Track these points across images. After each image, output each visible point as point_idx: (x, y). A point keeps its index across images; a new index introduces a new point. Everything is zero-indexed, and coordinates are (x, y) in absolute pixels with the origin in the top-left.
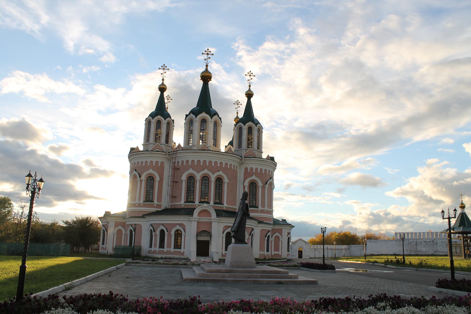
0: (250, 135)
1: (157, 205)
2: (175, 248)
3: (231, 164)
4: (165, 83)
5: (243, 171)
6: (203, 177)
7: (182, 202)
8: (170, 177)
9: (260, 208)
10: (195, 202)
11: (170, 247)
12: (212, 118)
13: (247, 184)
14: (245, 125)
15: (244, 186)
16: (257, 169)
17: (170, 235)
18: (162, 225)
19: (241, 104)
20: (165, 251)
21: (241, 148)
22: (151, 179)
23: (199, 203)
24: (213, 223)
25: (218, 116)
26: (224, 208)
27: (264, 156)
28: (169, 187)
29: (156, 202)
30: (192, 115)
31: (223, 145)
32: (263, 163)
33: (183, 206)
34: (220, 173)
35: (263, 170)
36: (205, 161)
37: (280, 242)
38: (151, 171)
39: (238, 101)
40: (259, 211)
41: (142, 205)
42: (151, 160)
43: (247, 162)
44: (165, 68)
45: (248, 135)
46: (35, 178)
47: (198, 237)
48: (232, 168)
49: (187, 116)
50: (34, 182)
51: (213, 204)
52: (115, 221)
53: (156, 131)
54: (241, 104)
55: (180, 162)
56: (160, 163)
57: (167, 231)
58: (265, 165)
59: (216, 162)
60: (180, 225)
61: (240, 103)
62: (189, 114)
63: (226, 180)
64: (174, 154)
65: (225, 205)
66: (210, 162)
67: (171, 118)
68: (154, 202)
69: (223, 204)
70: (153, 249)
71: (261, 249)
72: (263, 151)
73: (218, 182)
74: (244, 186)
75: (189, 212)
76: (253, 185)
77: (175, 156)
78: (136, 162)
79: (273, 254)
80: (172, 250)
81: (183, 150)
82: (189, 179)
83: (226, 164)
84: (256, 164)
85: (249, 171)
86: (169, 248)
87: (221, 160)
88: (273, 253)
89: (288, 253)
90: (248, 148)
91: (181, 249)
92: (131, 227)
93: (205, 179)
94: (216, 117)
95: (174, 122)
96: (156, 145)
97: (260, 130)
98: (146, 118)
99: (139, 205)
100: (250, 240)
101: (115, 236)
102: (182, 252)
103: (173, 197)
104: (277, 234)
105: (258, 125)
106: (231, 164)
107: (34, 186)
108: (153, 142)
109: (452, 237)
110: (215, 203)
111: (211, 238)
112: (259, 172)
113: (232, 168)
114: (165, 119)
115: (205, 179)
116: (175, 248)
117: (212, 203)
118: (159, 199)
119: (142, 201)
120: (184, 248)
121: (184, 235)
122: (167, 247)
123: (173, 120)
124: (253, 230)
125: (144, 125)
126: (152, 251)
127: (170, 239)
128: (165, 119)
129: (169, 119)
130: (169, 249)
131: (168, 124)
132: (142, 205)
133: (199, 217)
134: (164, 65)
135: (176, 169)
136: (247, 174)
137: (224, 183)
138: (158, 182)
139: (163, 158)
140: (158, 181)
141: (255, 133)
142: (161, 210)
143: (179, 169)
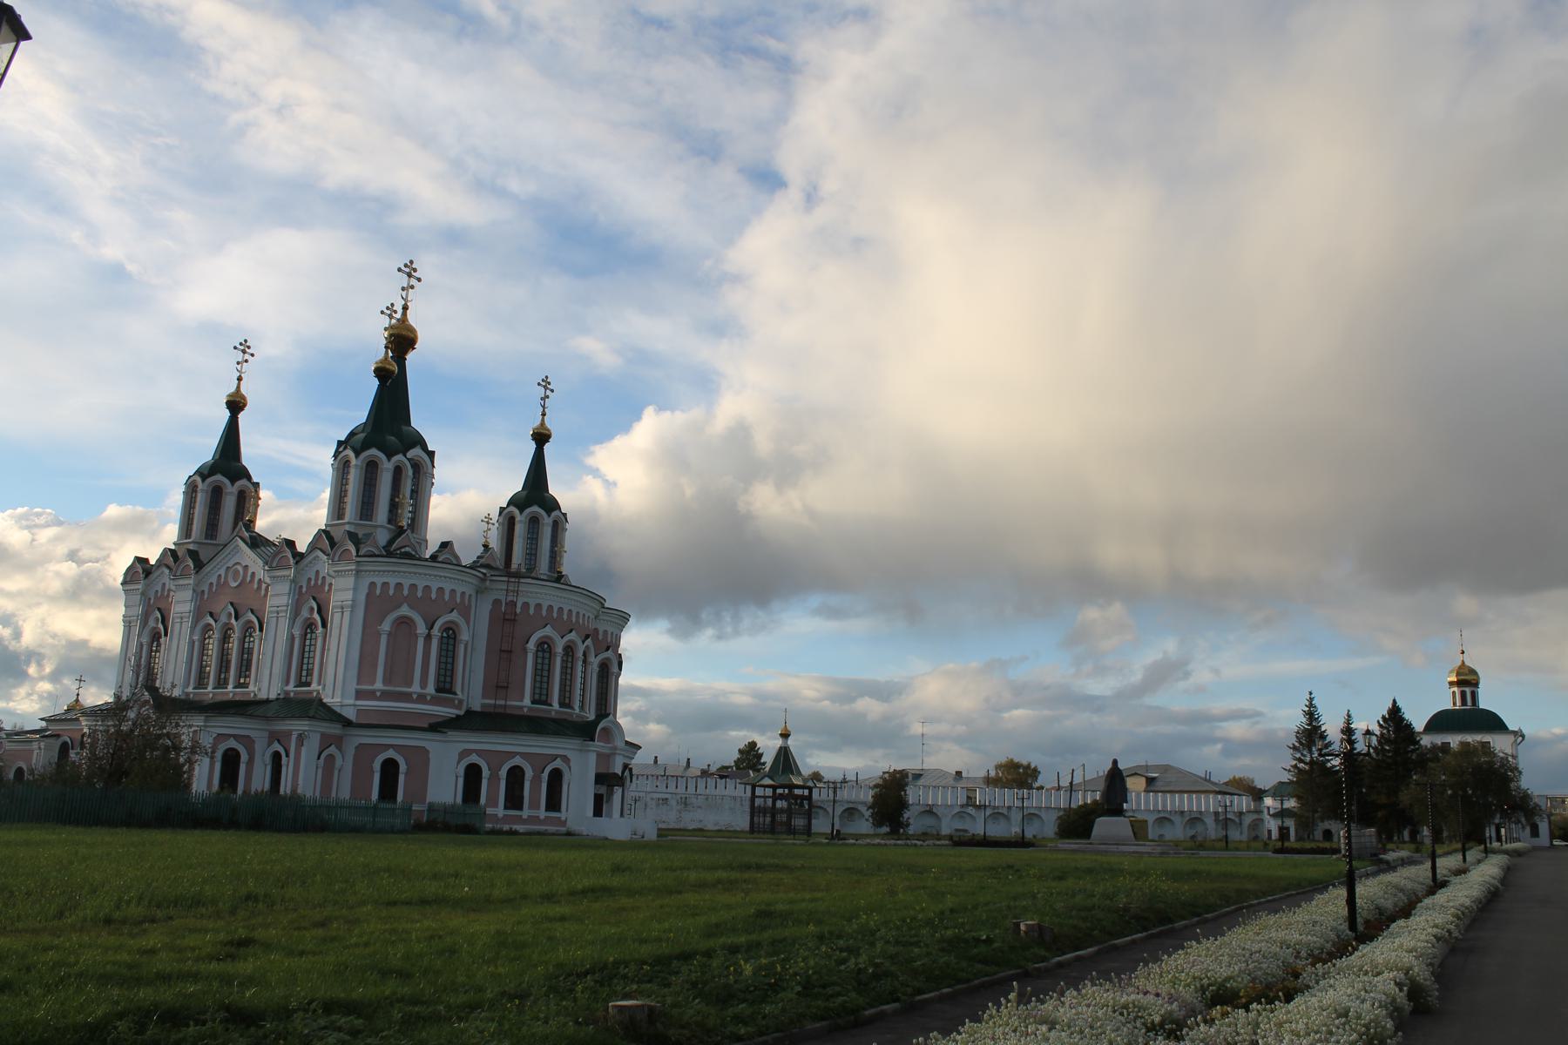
2: (506, 808)
7: (527, 701)
11: (538, 808)
14: (389, 457)
17: (494, 777)
19: (252, 355)
20: (525, 817)
21: (371, 520)
30: (512, 508)
33: (525, 710)
39: (246, 341)
42: (453, 587)
48: (565, 617)
54: (252, 355)
69: (551, 705)
73: (540, 654)
80: (500, 811)
83: (561, 609)
86: (534, 810)
87: (222, 566)
109: (802, 784)
113: (565, 617)
119: (431, 689)
120: (567, 811)
122: (530, 807)
130: (533, 813)
137: (555, 656)
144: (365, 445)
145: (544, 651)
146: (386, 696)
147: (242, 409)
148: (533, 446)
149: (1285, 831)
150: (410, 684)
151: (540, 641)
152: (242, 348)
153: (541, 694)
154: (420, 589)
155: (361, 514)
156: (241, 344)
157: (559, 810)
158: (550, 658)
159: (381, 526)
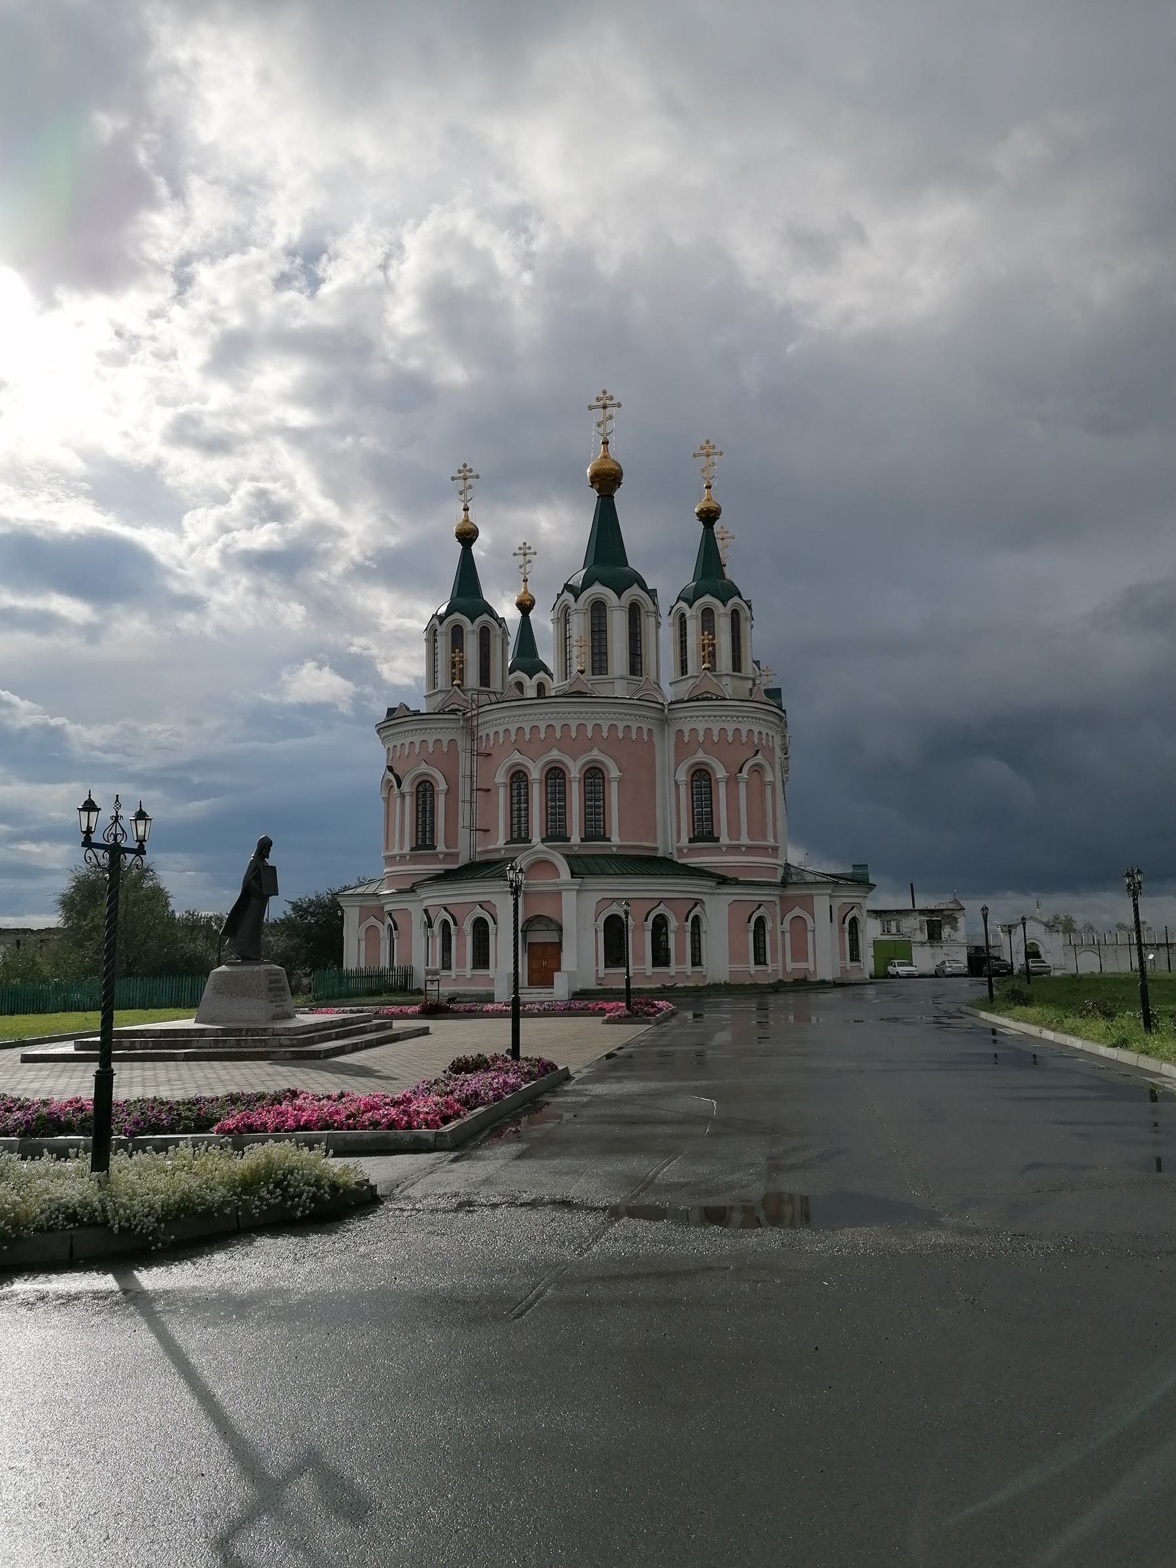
0: (457, 650)
1: (446, 854)
5: (673, 741)
7: (501, 843)
9: (725, 840)
10: (570, 838)
11: (643, 963)
13: (682, 776)
15: (676, 782)
18: (480, 906)
22: (425, 790)
25: (643, 585)
26: (615, 849)
29: (441, 847)
30: (682, 604)
32: (542, 711)
33: (503, 852)
37: (810, 935)
43: (676, 716)
44: (468, 474)
50: (113, 823)
51: (580, 840)
52: (360, 904)
58: (726, 717)
61: (532, 551)
67: (741, 598)
68: (437, 848)
69: (609, 840)
71: (735, 955)
78: (398, 743)
79: (789, 970)
80: (468, 971)
81: (492, 704)
82: (515, 780)
84: (724, 718)
88: (791, 966)
89: (597, 968)
91: (451, 970)
93: (555, 774)
94: (635, 590)
95: (750, 607)
96: (452, 692)
102: (810, 970)
104: (797, 911)
107: (116, 836)
108: (446, 687)
111: (561, 936)
114: (724, 603)
118: (451, 839)
119: (407, 849)
120: (496, 967)
121: (495, 931)
126: (454, 977)
127: (640, 943)
129: (736, 599)
131: (735, 616)
132: (685, 851)
134: (465, 466)
138: (446, 794)
139: (453, 729)
140: (445, 792)
141: (723, 626)
142: (459, 868)
144: (698, 593)
146: (750, 850)
147: (715, 518)
149: (936, 936)
150: (764, 838)
152: (522, 551)
154: (730, 733)
155: (593, 668)
159: (727, 675)
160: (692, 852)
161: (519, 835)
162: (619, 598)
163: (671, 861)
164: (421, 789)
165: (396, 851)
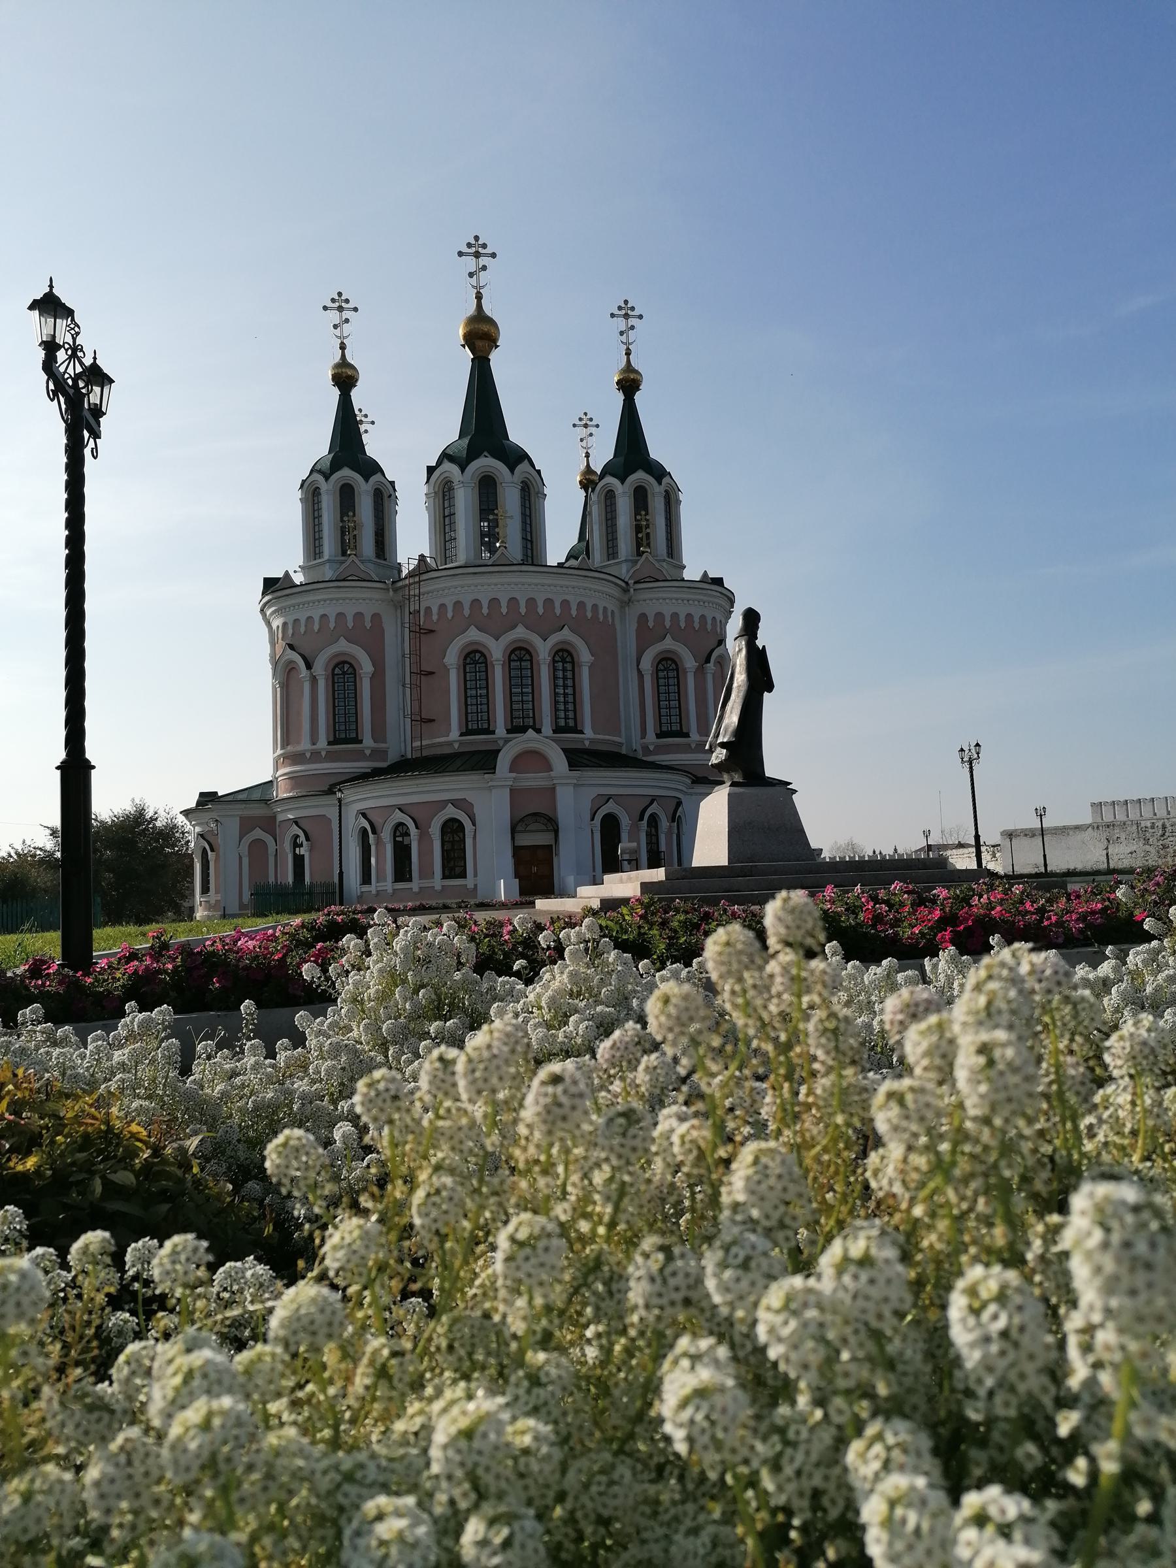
2: (444, 877)
3: (595, 607)
4: (349, 359)
5: (635, 626)
6: (513, 652)
7: (454, 734)
8: (407, 660)
12: (512, 470)
13: (647, 663)
15: (639, 671)
16: (675, 616)
17: (424, 835)
23: (509, 731)
24: (558, 789)
26: (587, 743)
27: (692, 573)
28: (408, 691)
29: (368, 742)
30: (447, 466)
31: (556, 549)
33: (456, 746)
34: (566, 634)
35: (696, 619)
36: (513, 601)
38: (343, 646)
40: (693, 746)
41: (323, 754)
45: (637, 513)
46: (74, 340)
47: (517, 836)
49: (431, 470)
53: (342, 521)
55: (435, 610)
56: (368, 619)
57: (417, 827)
59: (549, 602)
60: (455, 803)
62: (440, 462)
63: (585, 656)
64: (415, 583)
65: (589, 734)
66: (531, 602)
70: (373, 888)
72: (684, 562)
74: (639, 671)
75: (484, 761)
76: (668, 665)
77: (417, 591)
80: (437, 882)
85: (651, 624)
90: (640, 554)
92: (295, 827)
93: (520, 655)
94: (523, 467)
97: (671, 500)
98: (304, 482)
99: (315, 756)
100: (675, 836)
101: (246, 861)
103: (423, 721)
105: (666, 480)
106: (595, 607)
110: (557, 730)
112: (683, 625)
115: (520, 655)
116: (444, 877)
117: (547, 729)
118: (379, 732)
119: (322, 743)
120: (476, 875)
123: (392, 483)
124: (679, 804)
125: (299, 505)
128: (367, 480)
129: (377, 477)
130: (426, 883)
133: (514, 775)
135: (421, 632)
136: (647, 633)
137: (580, 666)
141: (657, 504)
143: (432, 631)
145: (476, 663)
148: (620, 397)
151: (467, 651)
153: (566, 718)
156: (333, 300)
157: (463, 875)
158: (573, 670)
160: (659, 750)
161: (477, 723)
162: (463, 471)
163: (636, 759)
164: (337, 671)
165: (305, 745)
